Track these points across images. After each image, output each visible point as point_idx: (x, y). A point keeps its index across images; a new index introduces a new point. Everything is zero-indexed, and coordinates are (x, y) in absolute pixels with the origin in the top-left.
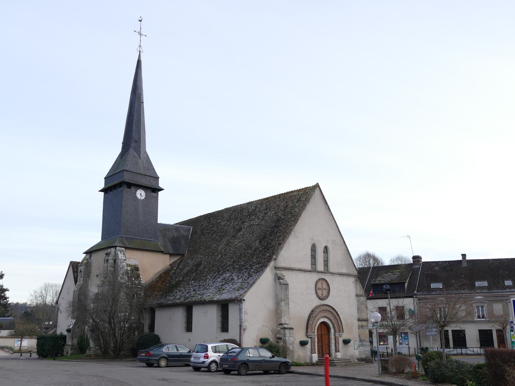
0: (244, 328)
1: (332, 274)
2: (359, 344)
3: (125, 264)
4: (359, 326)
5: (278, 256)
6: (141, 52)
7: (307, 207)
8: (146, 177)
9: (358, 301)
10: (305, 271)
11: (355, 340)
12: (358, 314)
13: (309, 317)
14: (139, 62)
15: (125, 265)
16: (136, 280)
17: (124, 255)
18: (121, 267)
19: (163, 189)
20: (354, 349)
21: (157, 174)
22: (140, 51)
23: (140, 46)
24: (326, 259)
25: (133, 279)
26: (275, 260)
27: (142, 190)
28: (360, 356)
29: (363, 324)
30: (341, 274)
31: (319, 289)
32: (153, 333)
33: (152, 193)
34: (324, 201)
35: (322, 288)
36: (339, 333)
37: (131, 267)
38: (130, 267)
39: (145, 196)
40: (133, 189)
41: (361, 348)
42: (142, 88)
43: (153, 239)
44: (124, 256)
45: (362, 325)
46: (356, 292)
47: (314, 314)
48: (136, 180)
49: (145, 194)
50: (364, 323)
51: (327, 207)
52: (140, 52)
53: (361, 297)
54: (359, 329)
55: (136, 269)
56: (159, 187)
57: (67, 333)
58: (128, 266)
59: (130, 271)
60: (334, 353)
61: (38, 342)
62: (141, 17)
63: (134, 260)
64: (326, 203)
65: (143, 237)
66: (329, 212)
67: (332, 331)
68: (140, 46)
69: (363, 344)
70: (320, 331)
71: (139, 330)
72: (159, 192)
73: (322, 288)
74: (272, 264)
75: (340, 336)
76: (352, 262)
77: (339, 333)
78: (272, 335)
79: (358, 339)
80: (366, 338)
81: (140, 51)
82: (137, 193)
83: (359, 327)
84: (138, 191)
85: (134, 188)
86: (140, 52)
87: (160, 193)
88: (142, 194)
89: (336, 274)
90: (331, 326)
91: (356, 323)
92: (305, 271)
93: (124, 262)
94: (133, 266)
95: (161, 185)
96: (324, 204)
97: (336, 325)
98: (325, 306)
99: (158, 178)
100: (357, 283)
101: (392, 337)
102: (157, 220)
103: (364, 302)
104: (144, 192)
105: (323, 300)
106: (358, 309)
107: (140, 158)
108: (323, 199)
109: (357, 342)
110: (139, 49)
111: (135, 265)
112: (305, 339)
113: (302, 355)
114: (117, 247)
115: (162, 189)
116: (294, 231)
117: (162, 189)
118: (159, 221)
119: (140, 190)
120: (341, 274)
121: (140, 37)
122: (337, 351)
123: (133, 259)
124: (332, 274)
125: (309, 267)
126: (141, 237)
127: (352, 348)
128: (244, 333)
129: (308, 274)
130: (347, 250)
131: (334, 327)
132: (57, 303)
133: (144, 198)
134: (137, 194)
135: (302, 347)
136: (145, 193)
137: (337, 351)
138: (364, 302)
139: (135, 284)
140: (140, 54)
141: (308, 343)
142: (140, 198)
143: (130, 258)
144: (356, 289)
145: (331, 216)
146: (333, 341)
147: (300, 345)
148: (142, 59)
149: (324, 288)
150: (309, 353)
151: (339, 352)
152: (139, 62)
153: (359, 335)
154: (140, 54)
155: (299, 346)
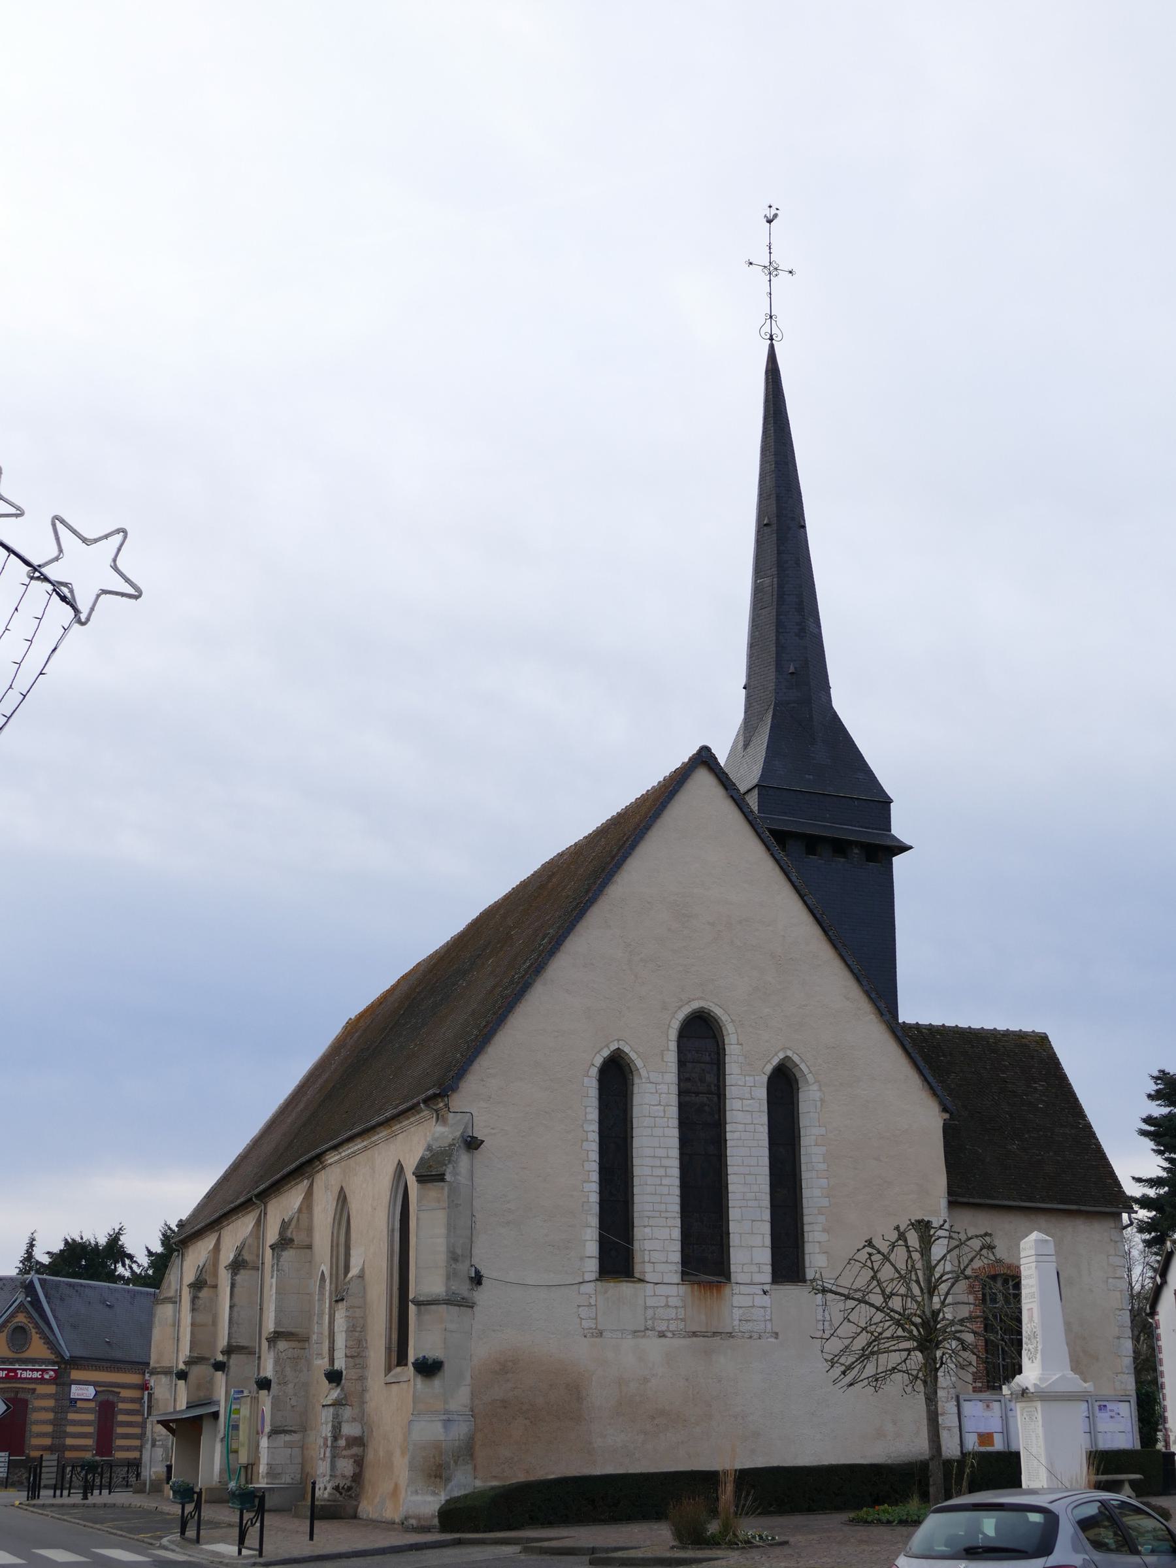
6: (774, 337)
19: (911, 848)
22: (771, 336)
23: (771, 317)
24: (86, 1505)
32: (1154, 1449)
42: (752, 587)
52: (771, 339)
57: (1018, 1385)
61: (1097, 1513)
68: (771, 317)
72: (894, 859)
81: (771, 336)
86: (771, 339)
87: (897, 860)
99: (887, 802)
101: (74, 1387)
110: (767, 328)
115: (904, 848)
117: (904, 848)
132: (360, 1519)
140: (772, 347)
154: (772, 347)
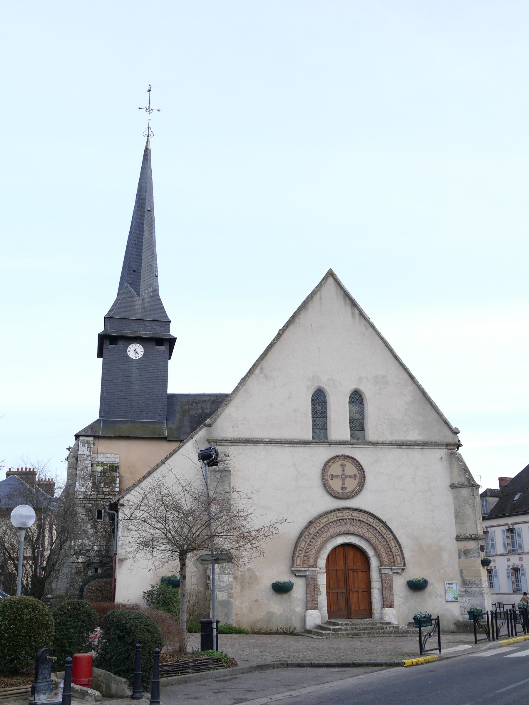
0: (120, 557)
1: (375, 444)
2: (461, 591)
3: (88, 462)
4: (460, 551)
5: (216, 420)
6: (150, 136)
7: (299, 319)
8: (146, 322)
9: (456, 498)
10: (305, 443)
11: (446, 582)
12: (456, 525)
13: (301, 534)
14: (147, 153)
15: (88, 464)
16: (107, 486)
17: (89, 449)
18: (81, 467)
20: (444, 602)
21: (167, 316)
23: (149, 128)
25: (102, 485)
26: (209, 425)
27: (138, 345)
28: (464, 618)
29: (468, 548)
30: (400, 445)
31: (333, 477)
33: (157, 347)
34: (348, 302)
35: (343, 474)
36: (390, 567)
37: (104, 467)
38: (103, 466)
39: (142, 353)
40: (121, 344)
41: (464, 598)
43: (158, 419)
44: (89, 450)
45: (465, 550)
46: (451, 478)
47: (313, 529)
48: (127, 329)
49: (143, 350)
50: (472, 545)
51: (357, 312)
52: (148, 137)
53: (462, 489)
54: (460, 558)
55: (114, 468)
56: (170, 335)
58: (100, 465)
59: (101, 472)
60: (379, 610)
62: (150, 85)
63: (112, 455)
64: (354, 304)
65: (140, 419)
66: (363, 322)
67: (374, 562)
68: (149, 128)
69: (469, 590)
70: (342, 563)
71: (105, 568)
73: (343, 474)
74: (201, 434)
75: (393, 573)
76: (438, 417)
77: (390, 567)
78: (195, 572)
79: (458, 581)
80: (475, 577)
82: (128, 349)
83: (459, 554)
84: (130, 346)
85: (123, 342)
86: (148, 137)
88: (137, 351)
89: (384, 444)
90: (370, 552)
91: (453, 546)
92: (305, 443)
93: (86, 459)
94: (108, 465)
95: (173, 332)
96: (349, 309)
97: (382, 550)
98: (347, 511)
99: (170, 322)
100: (453, 459)
102: (166, 388)
103: (469, 499)
104: (141, 347)
105: (353, 497)
106: (457, 516)
107: (138, 294)
108: (344, 299)
109: (454, 586)
111: (111, 464)
112: (284, 578)
113: (279, 613)
114: (80, 437)
116: (262, 368)
118: (173, 388)
119: (134, 345)
120: (400, 445)
121: (149, 114)
122: (388, 604)
123: (111, 454)
124: (375, 444)
125: (308, 435)
126: (136, 418)
127: (439, 599)
128: (121, 566)
129: (302, 448)
130: (421, 394)
131: (378, 555)
133: (140, 356)
134: (129, 351)
135: (279, 596)
136: (143, 348)
137: (388, 604)
138: (469, 499)
139: (103, 493)
141: (293, 586)
142: (133, 358)
143: (105, 452)
144: (451, 473)
145: (371, 329)
146: (376, 585)
147: (274, 592)
148: (152, 147)
149: (347, 475)
150: (299, 609)
151: (391, 606)
152: (147, 153)
153: (461, 571)
154: (148, 140)
155: (271, 594)
